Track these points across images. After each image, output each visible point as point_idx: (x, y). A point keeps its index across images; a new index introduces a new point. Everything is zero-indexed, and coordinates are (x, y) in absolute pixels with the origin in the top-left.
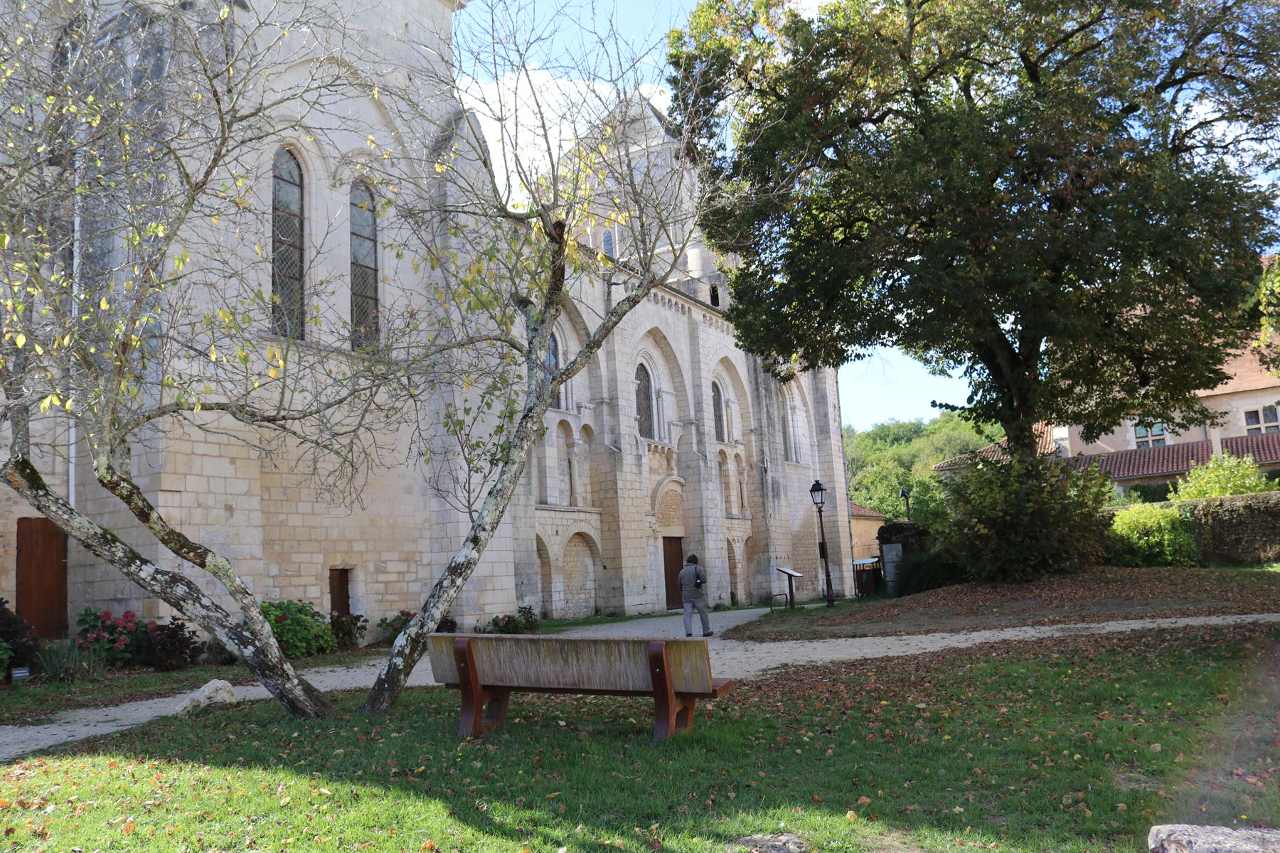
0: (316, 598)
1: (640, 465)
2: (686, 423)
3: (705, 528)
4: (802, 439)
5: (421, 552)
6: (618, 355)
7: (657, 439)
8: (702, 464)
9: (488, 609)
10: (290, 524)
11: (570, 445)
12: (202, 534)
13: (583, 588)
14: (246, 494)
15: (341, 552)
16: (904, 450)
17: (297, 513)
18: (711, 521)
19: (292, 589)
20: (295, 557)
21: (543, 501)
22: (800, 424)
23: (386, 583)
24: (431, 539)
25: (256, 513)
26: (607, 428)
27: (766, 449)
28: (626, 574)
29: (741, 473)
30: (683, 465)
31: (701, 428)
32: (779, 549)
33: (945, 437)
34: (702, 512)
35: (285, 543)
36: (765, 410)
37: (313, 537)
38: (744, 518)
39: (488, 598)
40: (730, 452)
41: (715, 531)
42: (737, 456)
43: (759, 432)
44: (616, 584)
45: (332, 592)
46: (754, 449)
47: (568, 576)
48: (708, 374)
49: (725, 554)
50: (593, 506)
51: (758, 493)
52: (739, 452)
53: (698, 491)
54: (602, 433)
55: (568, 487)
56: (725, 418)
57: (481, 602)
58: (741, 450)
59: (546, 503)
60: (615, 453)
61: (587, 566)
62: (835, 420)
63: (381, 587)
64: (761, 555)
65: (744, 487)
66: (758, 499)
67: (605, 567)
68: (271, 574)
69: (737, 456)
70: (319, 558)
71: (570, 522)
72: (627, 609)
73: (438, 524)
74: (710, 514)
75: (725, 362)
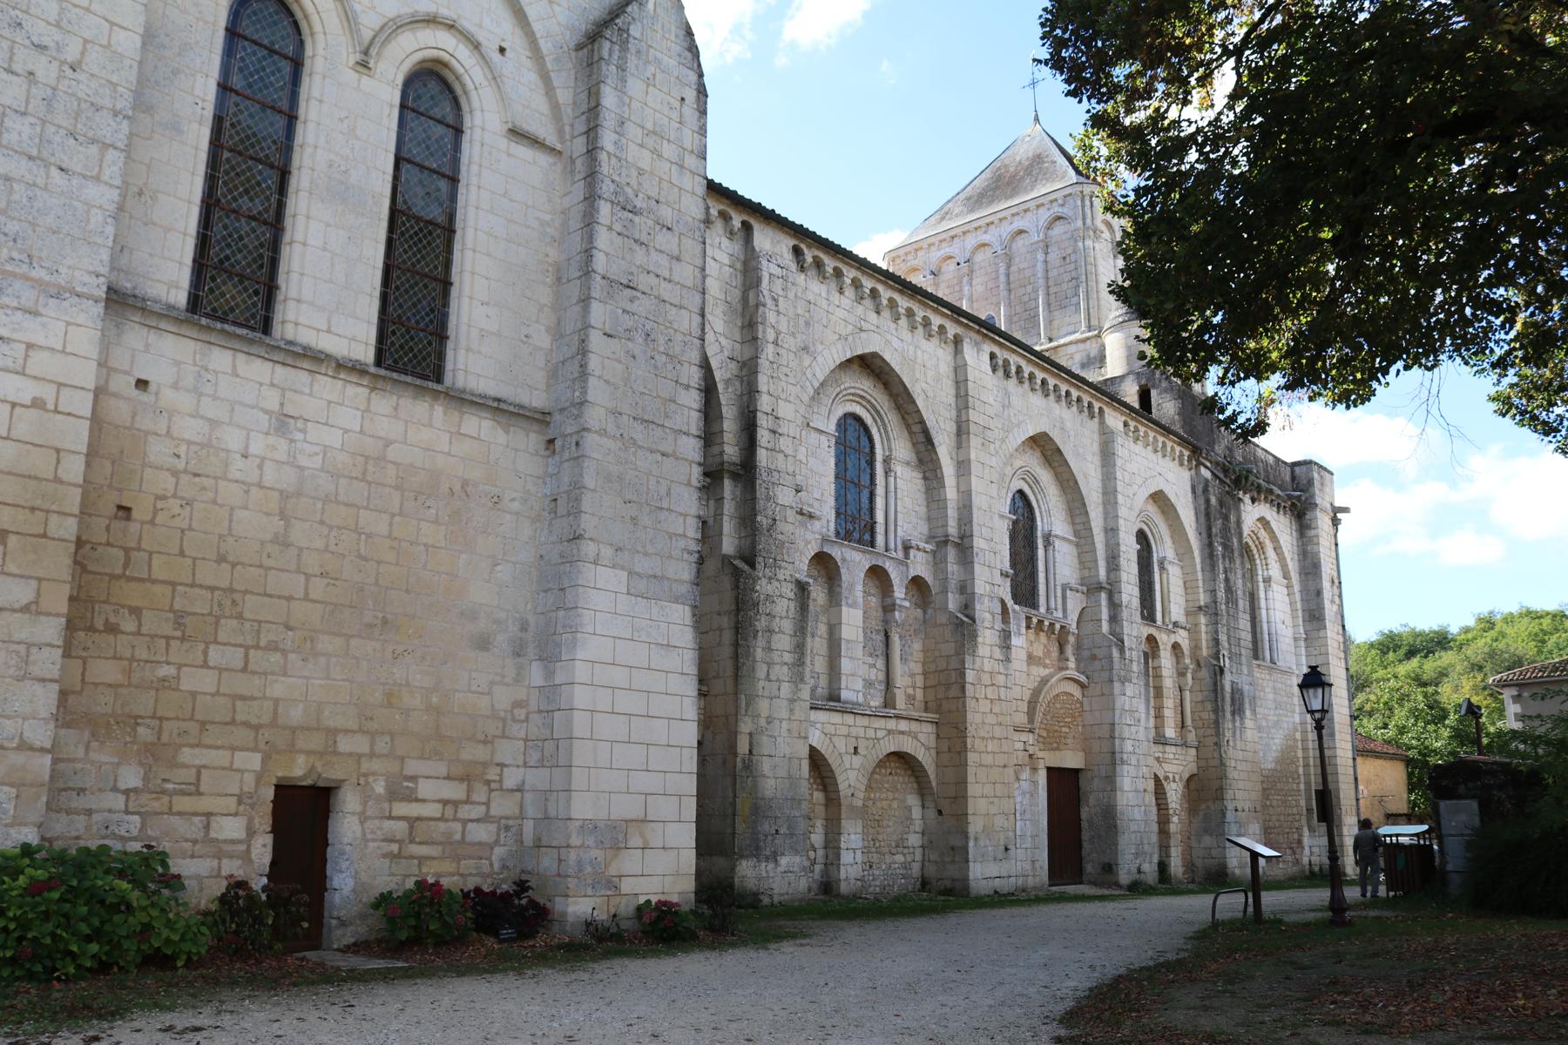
0: (233, 842)
1: (1008, 648)
2: (1092, 588)
3: (1118, 756)
4: (1281, 627)
5: (502, 765)
6: (975, 467)
7: (1042, 610)
8: (1115, 653)
9: (627, 886)
11: (888, 608)
13: (900, 844)
14: (25, 609)
15: (308, 753)
16: (1430, 666)
17: (205, 665)
18: (1128, 746)
19: (175, 820)
20: (187, 755)
21: (834, 697)
22: (1278, 605)
23: (413, 821)
24: (526, 740)
26: (952, 584)
27: (1223, 638)
28: (975, 826)
29: (1181, 674)
30: (1086, 654)
31: (1116, 596)
32: (1239, 795)
33: (1486, 650)
34: (1113, 730)
35: (166, 725)
36: (1222, 576)
37: (239, 718)
38: (1185, 745)
39: (629, 862)
40: (1165, 640)
41: (1134, 762)
42: (1176, 646)
43: (1212, 610)
44: (956, 841)
46: (1204, 636)
47: (873, 823)
48: (1132, 511)
49: (1150, 799)
50: (926, 710)
51: (1209, 706)
52: (1180, 640)
53: (1108, 698)
54: (945, 591)
55: (882, 676)
56: (1157, 587)
57: (613, 871)
58: (1182, 637)
59: (838, 700)
60: (964, 627)
61: (909, 809)
62: (1333, 602)
63: (400, 828)
64: (1210, 803)
65: (1187, 695)
66: (1208, 716)
67: (940, 813)
68: (122, 786)
69: (1176, 646)
70: (254, 761)
71: (880, 734)
72: (973, 884)
73: (540, 712)
74: (1126, 735)
75: (1159, 498)
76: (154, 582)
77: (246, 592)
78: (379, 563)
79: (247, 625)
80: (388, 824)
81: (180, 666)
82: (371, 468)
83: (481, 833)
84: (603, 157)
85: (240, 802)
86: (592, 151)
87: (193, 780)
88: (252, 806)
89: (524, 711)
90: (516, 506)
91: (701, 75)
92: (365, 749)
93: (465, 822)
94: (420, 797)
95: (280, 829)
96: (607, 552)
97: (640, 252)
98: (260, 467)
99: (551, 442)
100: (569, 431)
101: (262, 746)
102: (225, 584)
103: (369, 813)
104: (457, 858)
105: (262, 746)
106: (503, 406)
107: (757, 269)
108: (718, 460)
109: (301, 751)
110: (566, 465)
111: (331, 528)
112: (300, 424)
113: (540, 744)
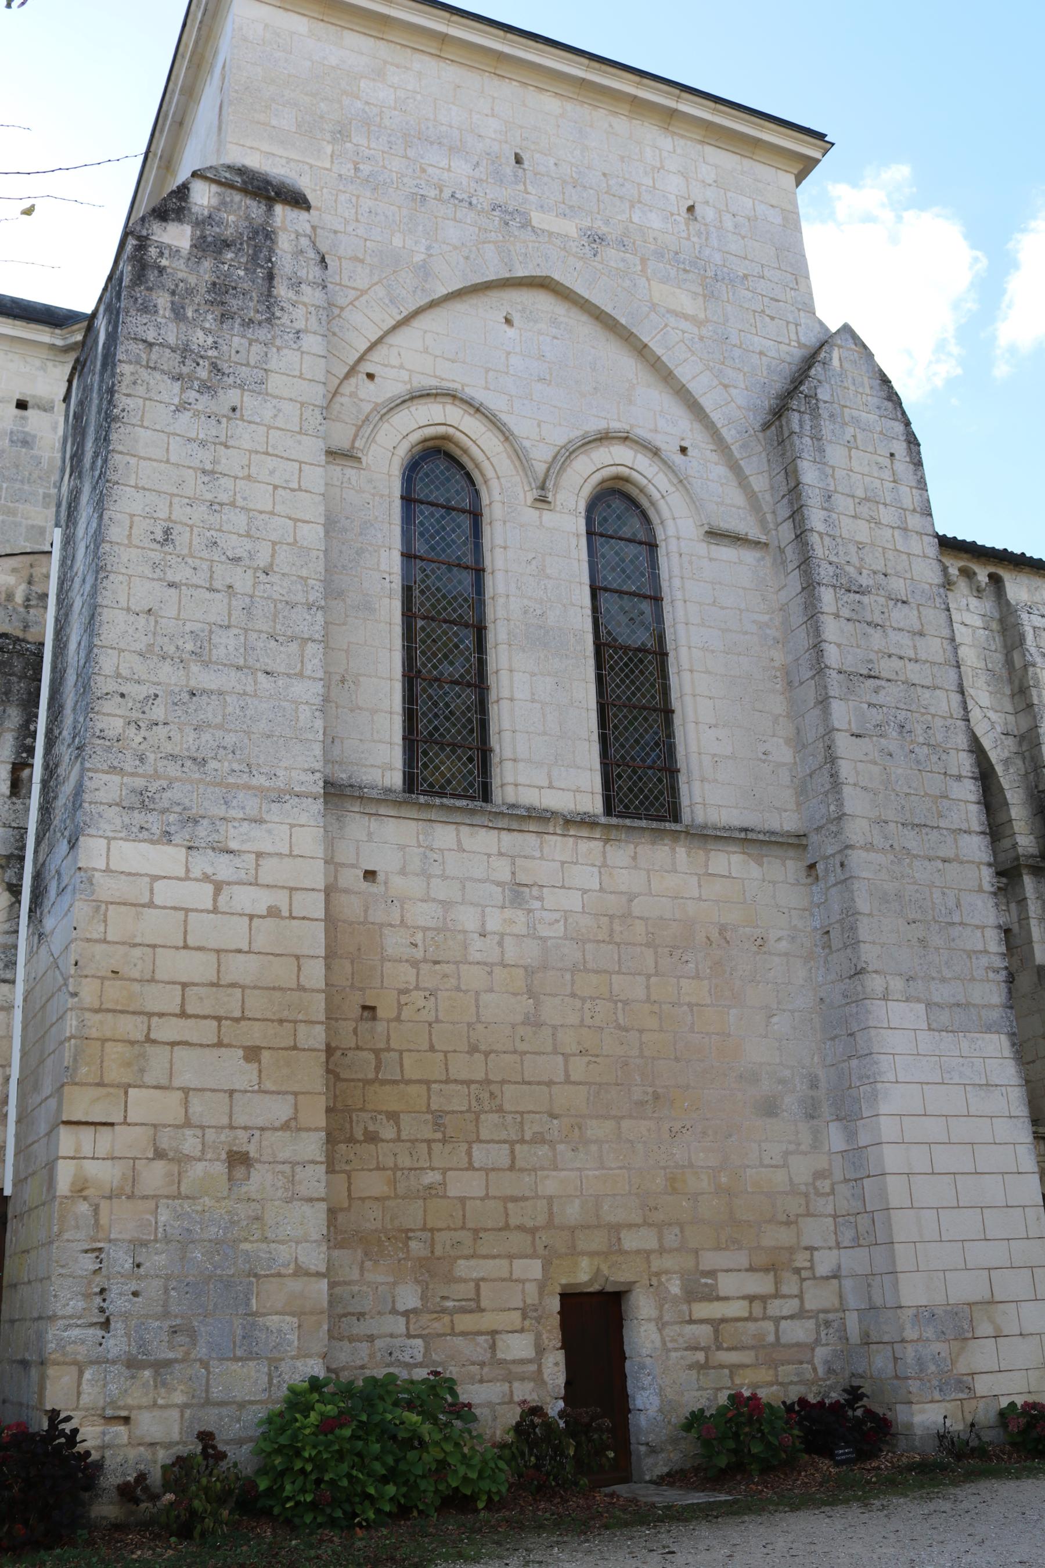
0: (522, 1362)
5: (811, 1249)
9: (983, 1386)
10: (451, 1193)
12: (162, 1219)
14: (285, 1127)
15: (592, 1254)
17: (471, 1167)
19: (459, 1341)
20: (463, 1268)
23: (717, 1324)
24: (835, 1217)
25: (310, 1168)
37: (513, 1221)
45: (567, 1345)
57: (962, 1368)
63: (703, 1332)
68: (401, 1308)
70: (534, 1269)
73: (846, 1181)
76: (408, 1082)
77: (503, 1082)
78: (641, 1031)
79: (509, 1118)
80: (689, 1329)
81: (444, 1171)
82: (617, 928)
83: (798, 1332)
84: (814, 539)
85: (524, 1317)
86: (801, 535)
87: (472, 1295)
88: (538, 1320)
89: (827, 1183)
90: (783, 945)
91: (908, 424)
92: (652, 1244)
93: (777, 1320)
94: (722, 1294)
95: (570, 1343)
96: (897, 984)
97: (876, 635)
98: (500, 944)
99: (812, 867)
100: (830, 852)
101: (540, 1251)
102: (480, 1076)
103: (667, 1318)
104: (774, 1365)
105: (540, 1251)
106: (750, 836)
107: (1018, 625)
108: (1011, 854)
109: (583, 1253)
110: (833, 890)
111: (583, 1000)
112: (535, 891)
113: (852, 1219)
